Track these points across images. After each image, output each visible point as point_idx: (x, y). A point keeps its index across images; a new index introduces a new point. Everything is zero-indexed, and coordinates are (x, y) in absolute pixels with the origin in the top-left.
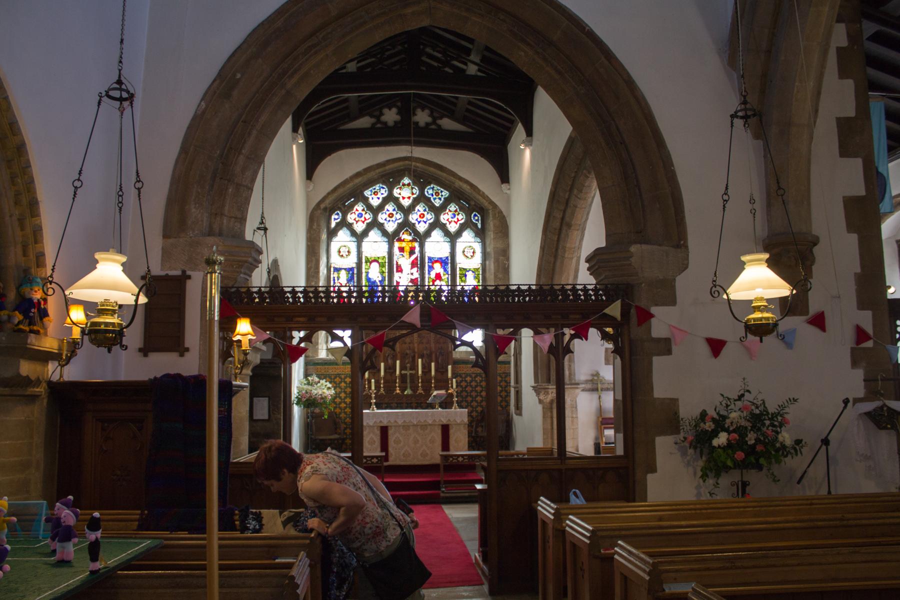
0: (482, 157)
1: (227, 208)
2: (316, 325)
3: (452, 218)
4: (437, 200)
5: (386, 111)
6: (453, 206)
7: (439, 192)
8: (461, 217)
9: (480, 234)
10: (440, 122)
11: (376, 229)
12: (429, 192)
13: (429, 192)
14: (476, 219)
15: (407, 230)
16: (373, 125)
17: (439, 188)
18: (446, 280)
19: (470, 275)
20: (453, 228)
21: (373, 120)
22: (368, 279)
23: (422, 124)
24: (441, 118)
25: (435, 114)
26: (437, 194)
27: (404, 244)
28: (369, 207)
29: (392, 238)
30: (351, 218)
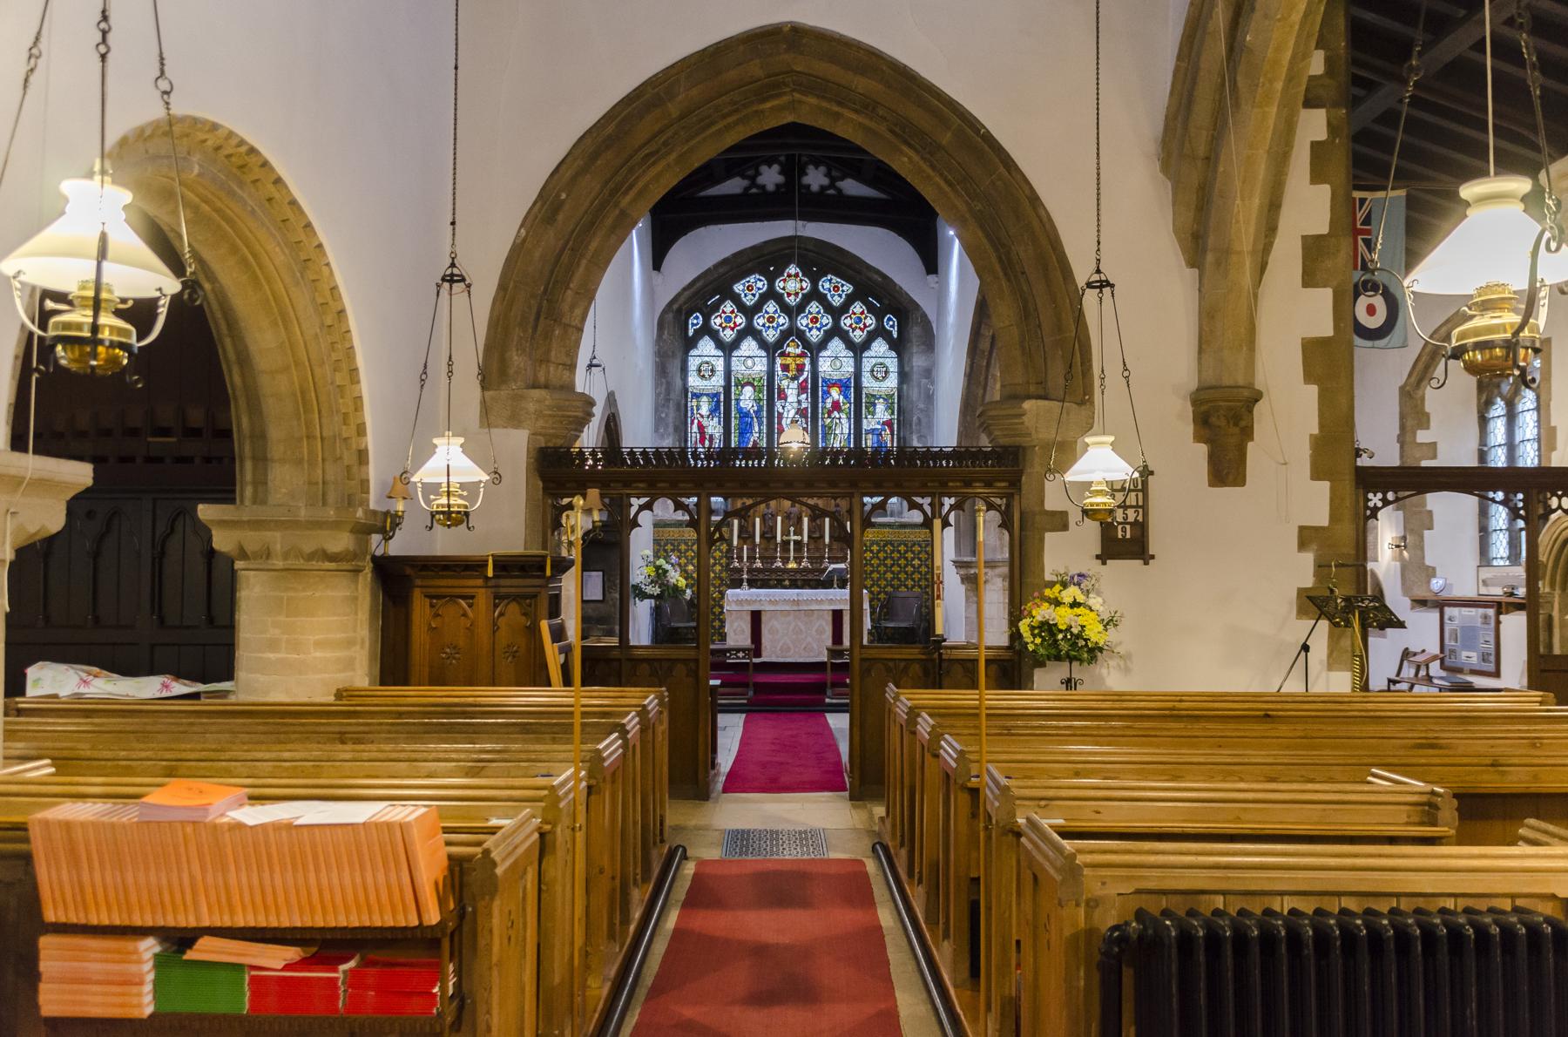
0: (899, 235)
1: (553, 353)
2: (658, 492)
3: (859, 319)
4: (837, 298)
5: (764, 169)
8: (871, 321)
9: (898, 346)
10: (840, 184)
11: (750, 338)
12: (825, 285)
13: (825, 285)
14: (891, 324)
15: (793, 341)
16: (747, 189)
19: (880, 407)
20: (858, 336)
21: (746, 183)
22: (740, 410)
23: (815, 188)
24: (842, 179)
25: (834, 173)
26: (836, 288)
27: (789, 361)
28: (741, 307)
29: (772, 350)
30: (716, 322)
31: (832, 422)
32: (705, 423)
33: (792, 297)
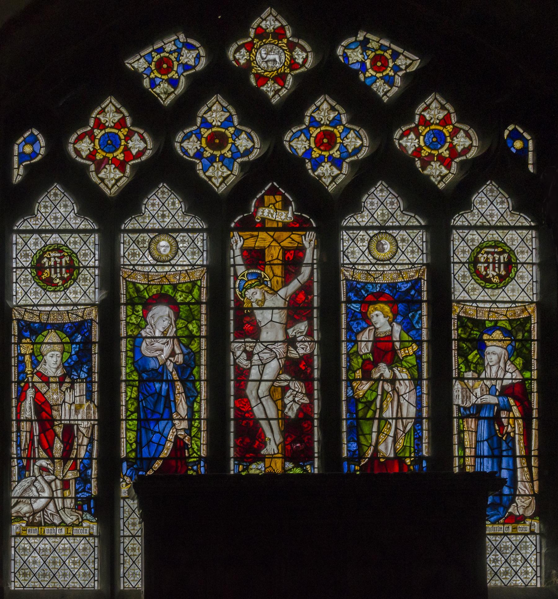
6: (111, 108)
7: (388, 55)
15: (273, 192)
17: (386, 43)
18: (413, 360)
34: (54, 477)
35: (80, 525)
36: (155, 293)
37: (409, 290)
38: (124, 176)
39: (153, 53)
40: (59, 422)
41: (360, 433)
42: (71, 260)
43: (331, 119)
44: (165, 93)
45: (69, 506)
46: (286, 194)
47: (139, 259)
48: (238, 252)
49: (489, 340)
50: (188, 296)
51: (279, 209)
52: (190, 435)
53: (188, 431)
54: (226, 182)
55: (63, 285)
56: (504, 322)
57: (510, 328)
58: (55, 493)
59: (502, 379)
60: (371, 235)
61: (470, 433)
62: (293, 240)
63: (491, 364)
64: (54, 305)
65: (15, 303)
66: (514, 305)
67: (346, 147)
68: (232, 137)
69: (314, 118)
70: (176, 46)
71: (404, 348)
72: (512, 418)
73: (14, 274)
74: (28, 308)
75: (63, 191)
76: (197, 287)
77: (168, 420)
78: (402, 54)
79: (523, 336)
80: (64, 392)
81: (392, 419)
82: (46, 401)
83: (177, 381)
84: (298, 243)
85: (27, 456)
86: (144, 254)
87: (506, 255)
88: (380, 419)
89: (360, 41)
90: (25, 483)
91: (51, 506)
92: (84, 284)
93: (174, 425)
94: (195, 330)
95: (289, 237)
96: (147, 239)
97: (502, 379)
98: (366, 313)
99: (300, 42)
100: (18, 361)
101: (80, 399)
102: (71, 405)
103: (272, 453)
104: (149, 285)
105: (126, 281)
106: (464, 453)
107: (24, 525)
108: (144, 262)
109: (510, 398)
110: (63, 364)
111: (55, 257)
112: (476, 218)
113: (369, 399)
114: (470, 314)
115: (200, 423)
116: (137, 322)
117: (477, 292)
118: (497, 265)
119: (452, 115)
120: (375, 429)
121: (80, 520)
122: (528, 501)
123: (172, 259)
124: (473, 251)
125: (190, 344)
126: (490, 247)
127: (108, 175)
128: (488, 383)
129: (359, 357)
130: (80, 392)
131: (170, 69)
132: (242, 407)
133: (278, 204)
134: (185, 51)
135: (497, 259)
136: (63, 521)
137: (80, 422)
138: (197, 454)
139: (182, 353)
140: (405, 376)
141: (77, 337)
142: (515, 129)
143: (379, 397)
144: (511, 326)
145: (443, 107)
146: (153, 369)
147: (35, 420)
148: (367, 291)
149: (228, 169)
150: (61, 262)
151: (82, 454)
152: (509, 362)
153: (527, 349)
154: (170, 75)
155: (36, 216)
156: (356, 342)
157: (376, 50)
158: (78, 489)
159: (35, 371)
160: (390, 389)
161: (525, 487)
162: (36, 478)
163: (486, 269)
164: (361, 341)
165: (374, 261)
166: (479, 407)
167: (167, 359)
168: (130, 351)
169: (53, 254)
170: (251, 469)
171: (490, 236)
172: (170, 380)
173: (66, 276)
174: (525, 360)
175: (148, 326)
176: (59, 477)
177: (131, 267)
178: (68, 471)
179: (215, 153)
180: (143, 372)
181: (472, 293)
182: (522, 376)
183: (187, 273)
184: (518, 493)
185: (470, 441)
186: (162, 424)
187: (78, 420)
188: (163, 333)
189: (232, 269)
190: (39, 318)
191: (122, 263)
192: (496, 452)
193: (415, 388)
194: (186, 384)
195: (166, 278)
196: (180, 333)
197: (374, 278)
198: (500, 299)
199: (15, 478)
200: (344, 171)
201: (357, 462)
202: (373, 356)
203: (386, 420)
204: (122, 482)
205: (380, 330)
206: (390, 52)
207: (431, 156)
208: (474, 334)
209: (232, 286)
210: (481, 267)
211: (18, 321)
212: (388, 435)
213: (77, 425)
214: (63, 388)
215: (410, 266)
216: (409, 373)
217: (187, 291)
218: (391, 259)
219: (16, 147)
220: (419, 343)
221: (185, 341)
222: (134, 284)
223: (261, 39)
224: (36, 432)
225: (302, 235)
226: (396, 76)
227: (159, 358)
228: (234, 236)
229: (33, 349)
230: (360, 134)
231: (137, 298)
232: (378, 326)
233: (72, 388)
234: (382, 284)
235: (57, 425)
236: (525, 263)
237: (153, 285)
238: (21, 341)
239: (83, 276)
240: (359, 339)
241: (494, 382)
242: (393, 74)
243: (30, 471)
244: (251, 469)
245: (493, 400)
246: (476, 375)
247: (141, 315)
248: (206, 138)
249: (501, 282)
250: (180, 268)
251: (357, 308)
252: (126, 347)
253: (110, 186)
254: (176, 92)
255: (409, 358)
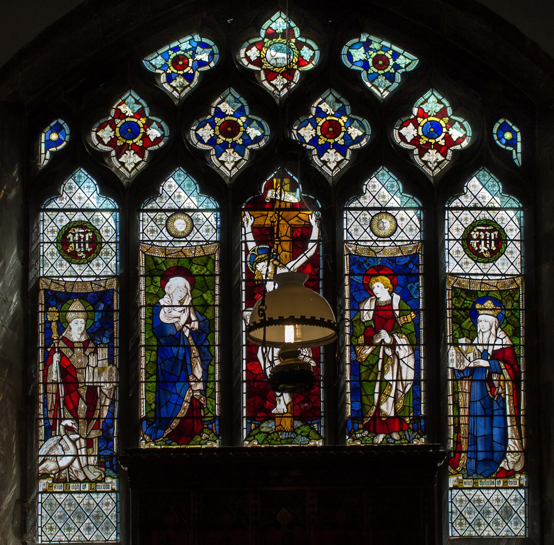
6: (131, 100)
11: (82, 173)
17: (388, 44)
31: (375, 354)
32: (77, 359)
33: (279, 82)
34: (78, 436)
35: (103, 481)
36: (172, 265)
37: (406, 265)
38: (143, 160)
39: (169, 51)
40: (83, 384)
41: (363, 394)
42: (94, 235)
43: (336, 110)
44: (181, 86)
45: (92, 463)
46: (294, 177)
47: (156, 235)
48: (249, 229)
49: (481, 309)
50: (203, 269)
51: (287, 191)
52: (205, 396)
53: (203, 392)
54: (237, 166)
55: (86, 258)
56: (494, 293)
57: (500, 299)
58: (79, 451)
59: (494, 345)
60: (373, 215)
61: (464, 394)
62: (300, 218)
63: (483, 331)
64: (78, 276)
65: (41, 275)
66: (504, 277)
67: (350, 135)
68: (243, 126)
69: (321, 109)
70: (191, 45)
71: (403, 316)
72: (502, 380)
73: (42, 248)
74: (54, 279)
75: (87, 174)
76: (211, 260)
77: (185, 382)
78: (402, 54)
79: (513, 306)
80: (88, 356)
81: (393, 381)
82: (71, 365)
83: (193, 346)
84: (305, 221)
85: (53, 416)
86: (161, 231)
87: (496, 233)
88: (382, 381)
89: (363, 42)
90: (51, 442)
91: (76, 462)
92: (105, 257)
93: (191, 386)
94: (210, 299)
95: (297, 216)
96: (164, 217)
97: (494, 345)
98: (368, 284)
99: (307, 41)
100: (45, 328)
101: (102, 363)
102: (94, 368)
103: (282, 412)
104: (166, 258)
105: (145, 255)
106: (459, 411)
107: (51, 482)
108: (161, 238)
109: (500, 362)
110: (87, 330)
111: (79, 233)
112: (469, 200)
113: (371, 362)
114: (463, 285)
115: (215, 385)
116: (155, 291)
117: (470, 266)
118: (488, 242)
119: (448, 109)
120: (377, 390)
121: (103, 476)
122: (517, 457)
123: (188, 235)
124: (466, 229)
125: (205, 311)
126: (482, 225)
127: (128, 159)
128: (480, 348)
129: (362, 324)
130: (103, 356)
131: (186, 65)
132: (254, 370)
133: (286, 186)
134: (199, 49)
135: (488, 236)
136: (87, 478)
137: (102, 384)
138: (212, 413)
139: (198, 320)
140: (404, 341)
141: (100, 306)
142: (505, 122)
143: (381, 361)
144: (502, 296)
145: (439, 102)
146: (171, 335)
147: (60, 383)
148: (369, 265)
149: (240, 155)
150: (85, 238)
151: (105, 413)
152: (500, 329)
153: (516, 317)
154: (185, 71)
155: (61, 196)
156: (359, 310)
157: (378, 51)
158: (101, 447)
159: (61, 337)
160: (390, 354)
161: (515, 443)
162: (62, 437)
163: (478, 245)
164: (364, 310)
165: (375, 238)
166: (472, 371)
167: (184, 326)
168: (150, 318)
169: (77, 230)
170: (263, 427)
171: (481, 216)
172: (187, 346)
173: (89, 250)
174: (514, 327)
175: (166, 296)
176: (83, 436)
177: (150, 243)
178: (92, 430)
179: (228, 140)
180: (162, 337)
181: (465, 266)
182: (512, 342)
183: (202, 248)
184: (508, 450)
185: (465, 401)
186: (179, 386)
187: (101, 382)
188: (180, 301)
189: (243, 244)
190: (65, 288)
191: (141, 239)
192: (488, 412)
193: (414, 352)
194: (201, 349)
195: (183, 252)
196: (195, 302)
197: (375, 253)
198: (490, 272)
199: (42, 437)
200: (348, 157)
201: (360, 420)
202: (374, 323)
203: (388, 381)
204: (142, 440)
205: (381, 300)
206: (391, 52)
207: (428, 144)
208: (467, 303)
209: (244, 260)
210: (474, 244)
211: (45, 290)
212: (389, 396)
213: (100, 386)
214: (87, 353)
215: (409, 243)
216: (408, 338)
217: (202, 264)
218: (391, 236)
219: (43, 135)
220: (417, 312)
221: (200, 309)
222: (153, 257)
223: (271, 39)
224: (62, 393)
225: (308, 215)
226: (397, 74)
227: (177, 325)
228: (245, 215)
229: (58, 316)
230: (362, 124)
231: (155, 270)
232: (378, 296)
233: (95, 352)
234: (382, 258)
235: (81, 387)
236: (514, 240)
237: (170, 258)
238: (48, 309)
239: (105, 250)
240: (362, 308)
241: (486, 348)
242: (394, 72)
243: (56, 430)
244: (263, 427)
245: (484, 363)
246: (469, 341)
247: (159, 285)
248: (220, 126)
249: (491, 257)
250: (195, 244)
251: (360, 280)
252: (145, 315)
253: (130, 169)
254: (191, 86)
255: (408, 325)
